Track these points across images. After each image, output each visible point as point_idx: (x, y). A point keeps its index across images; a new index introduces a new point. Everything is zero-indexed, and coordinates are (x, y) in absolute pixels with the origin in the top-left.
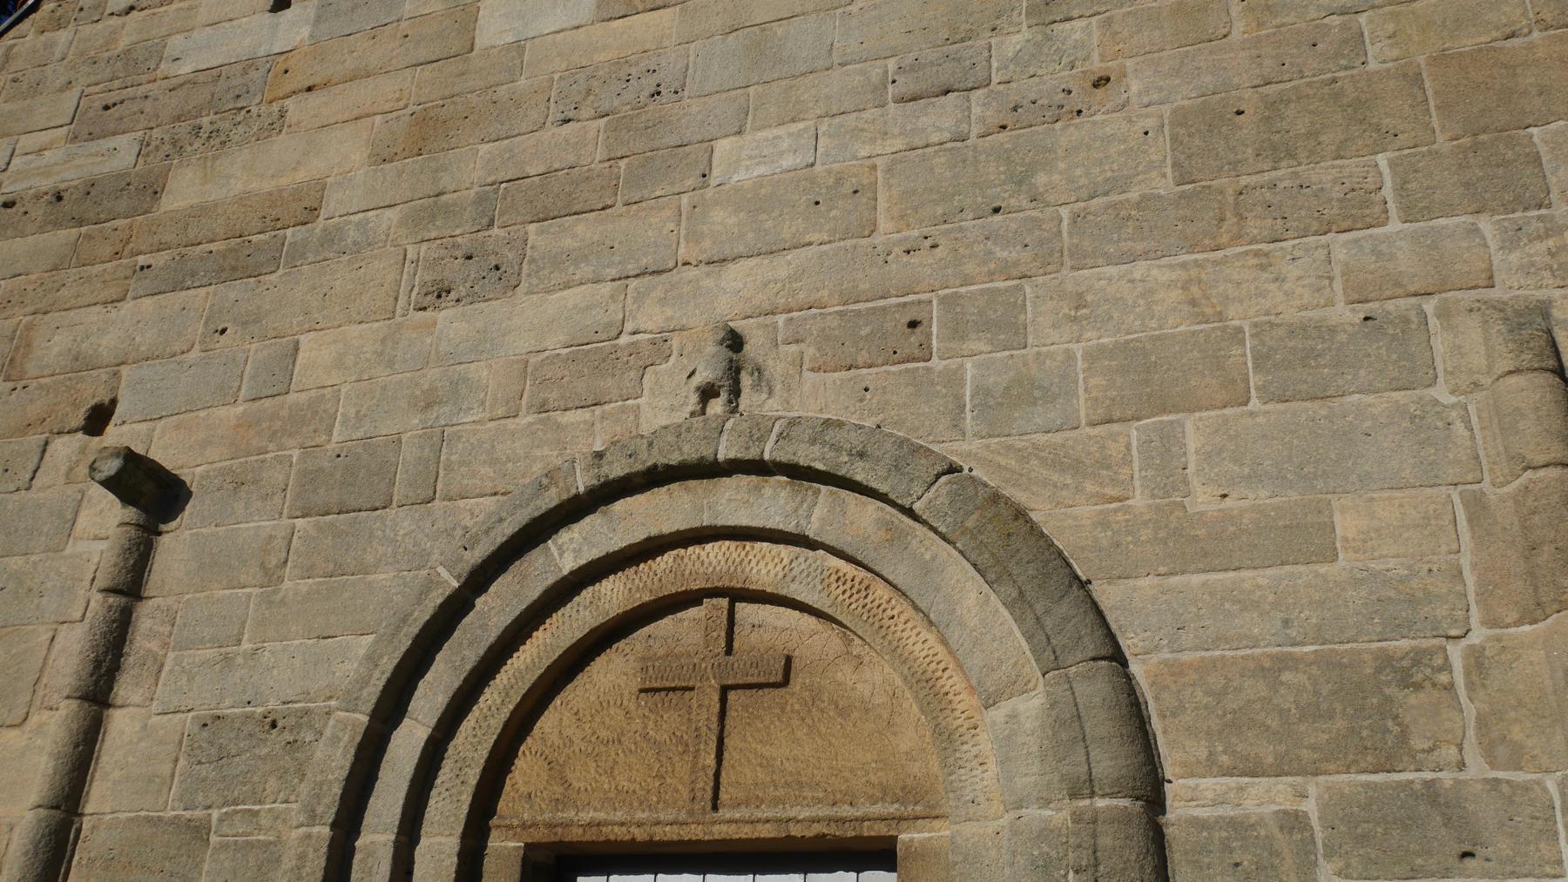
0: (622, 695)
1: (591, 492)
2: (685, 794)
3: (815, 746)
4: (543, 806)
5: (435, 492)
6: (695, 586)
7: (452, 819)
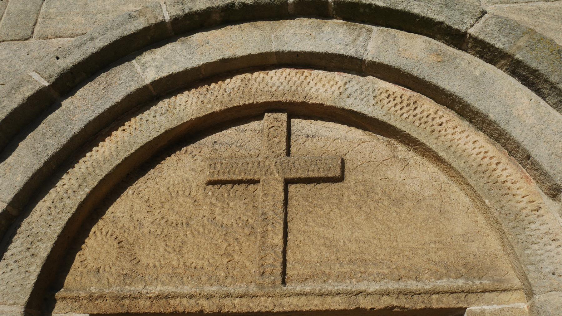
0: (190, 187)
1: (176, 21)
2: (253, 268)
3: (375, 229)
4: (111, 280)
5: (33, 33)
6: (260, 100)
7: (18, 289)
